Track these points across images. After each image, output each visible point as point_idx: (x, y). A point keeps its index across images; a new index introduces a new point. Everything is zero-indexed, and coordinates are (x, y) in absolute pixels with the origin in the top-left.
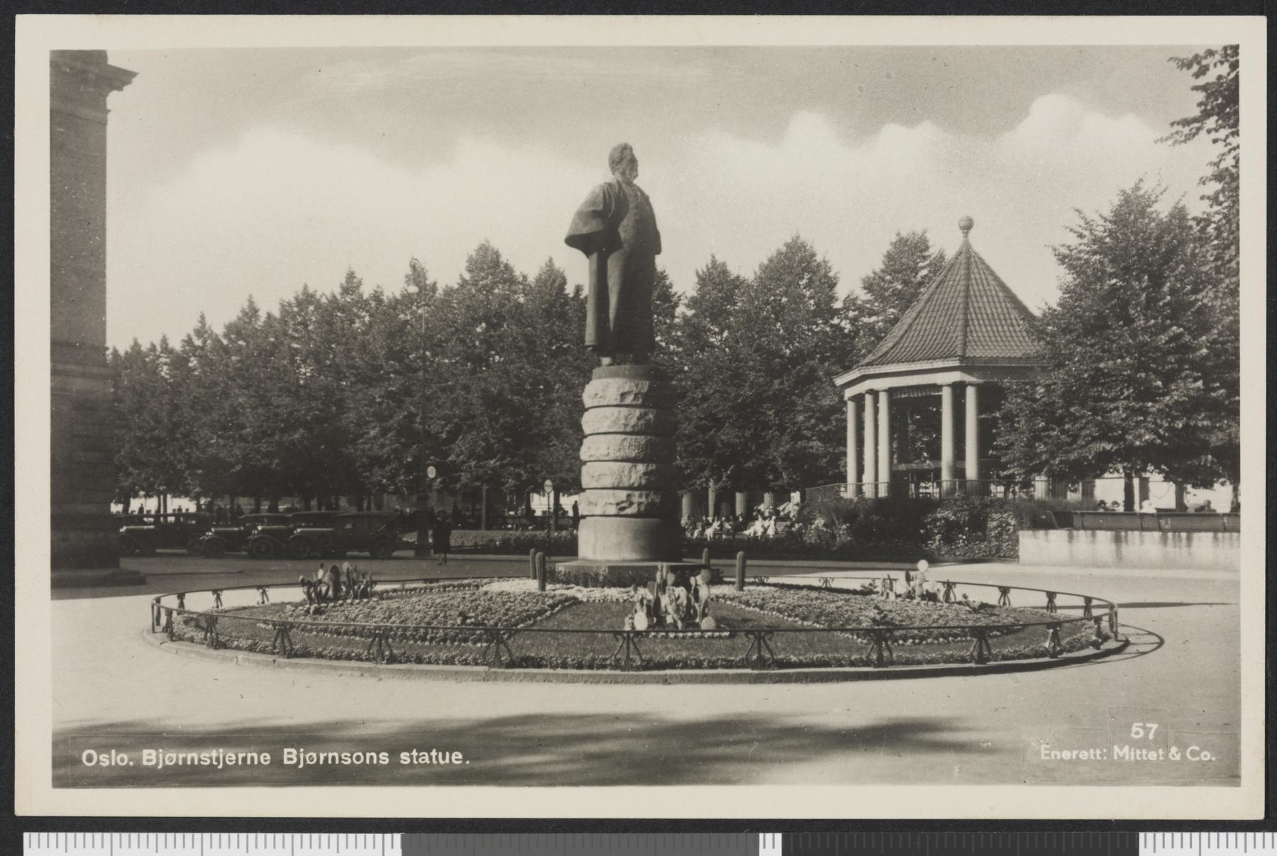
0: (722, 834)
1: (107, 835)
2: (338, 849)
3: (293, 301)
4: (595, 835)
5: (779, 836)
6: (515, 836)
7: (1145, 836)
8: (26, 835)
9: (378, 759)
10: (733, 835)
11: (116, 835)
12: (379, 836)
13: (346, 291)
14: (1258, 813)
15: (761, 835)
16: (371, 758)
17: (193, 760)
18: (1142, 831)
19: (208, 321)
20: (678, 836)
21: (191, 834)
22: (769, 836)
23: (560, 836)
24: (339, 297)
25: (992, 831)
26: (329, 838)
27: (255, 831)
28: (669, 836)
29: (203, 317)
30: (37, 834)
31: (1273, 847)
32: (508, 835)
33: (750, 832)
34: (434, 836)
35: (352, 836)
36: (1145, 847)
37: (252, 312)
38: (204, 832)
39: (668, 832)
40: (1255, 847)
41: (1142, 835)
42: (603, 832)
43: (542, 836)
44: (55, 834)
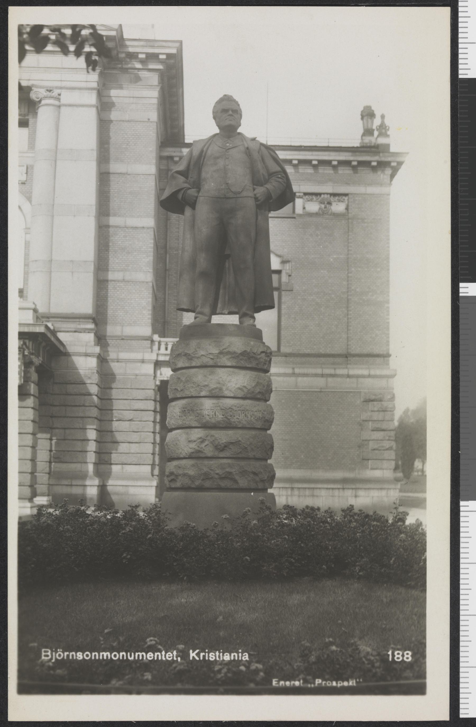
0: (460, 318)
1: (461, 670)
2: (469, 537)
5: (461, 285)
8: (461, 716)
9: (76, 656)
10: (461, 311)
11: (461, 664)
12: (462, 514)
14: (447, 10)
15: (461, 295)
16: (95, 655)
17: (107, 657)
18: (458, 76)
20: (461, 342)
22: (461, 290)
23: (461, 410)
25: (458, 162)
26: (463, 558)
27: (459, 584)
28: (461, 347)
30: (461, 617)
32: (461, 440)
33: (459, 301)
34: (461, 483)
35: (462, 530)
36: (467, 74)
38: (459, 645)
39: (459, 348)
41: (460, 77)
42: (459, 385)
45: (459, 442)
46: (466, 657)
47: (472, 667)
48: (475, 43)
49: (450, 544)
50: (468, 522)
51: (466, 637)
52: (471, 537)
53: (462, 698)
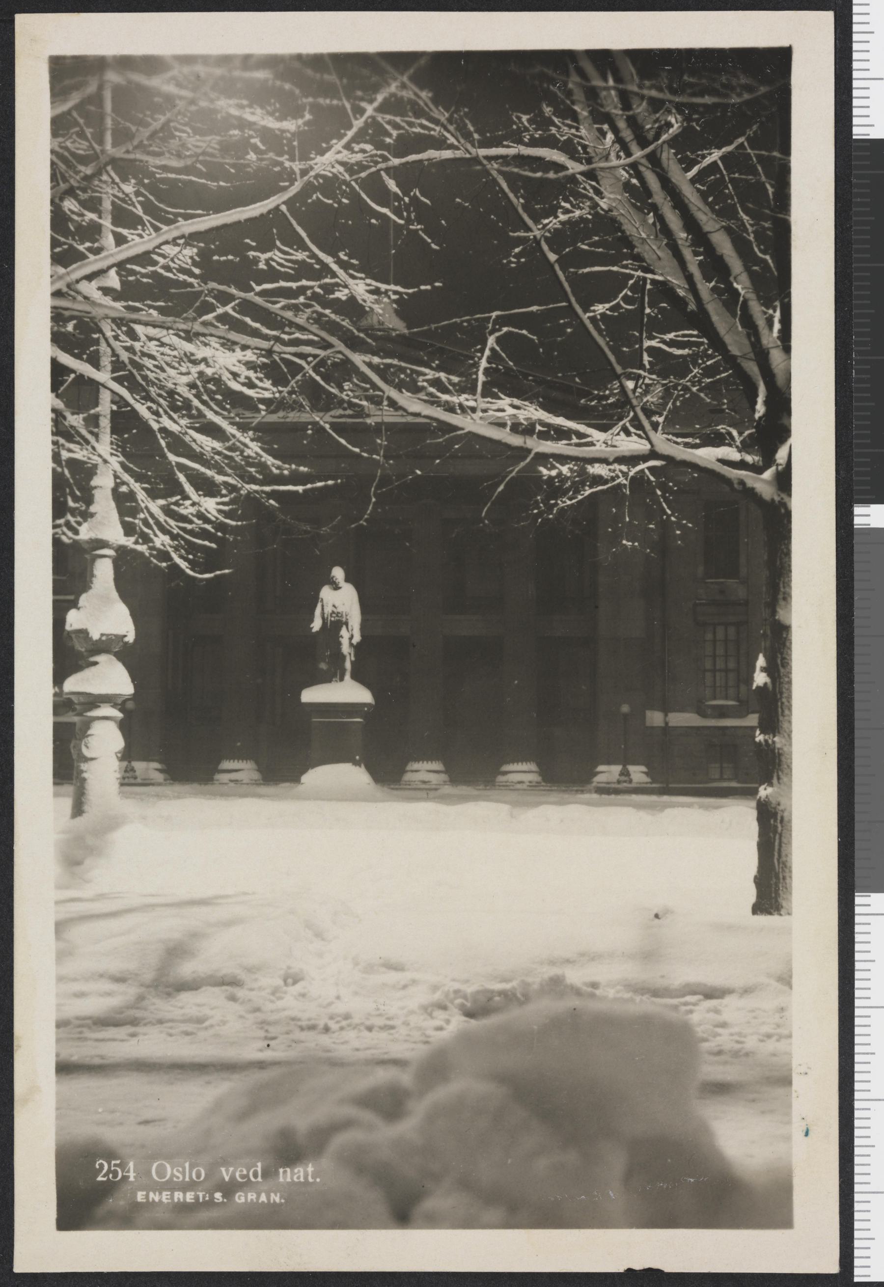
0: (856, 773)
3: (125, 764)
5: (858, 510)
7: (857, 1276)
14: (826, 19)
21: (856, 982)
22: (857, 521)
27: (853, 1072)
31: (869, 979)
40: (868, 51)
44: (856, 1000)
45: (853, 761)
47: (880, 1100)
48: (882, 79)
49: (834, 488)
50: (868, 70)
51: (864, 1185)
52: (874, 961)
53: (858, 970)
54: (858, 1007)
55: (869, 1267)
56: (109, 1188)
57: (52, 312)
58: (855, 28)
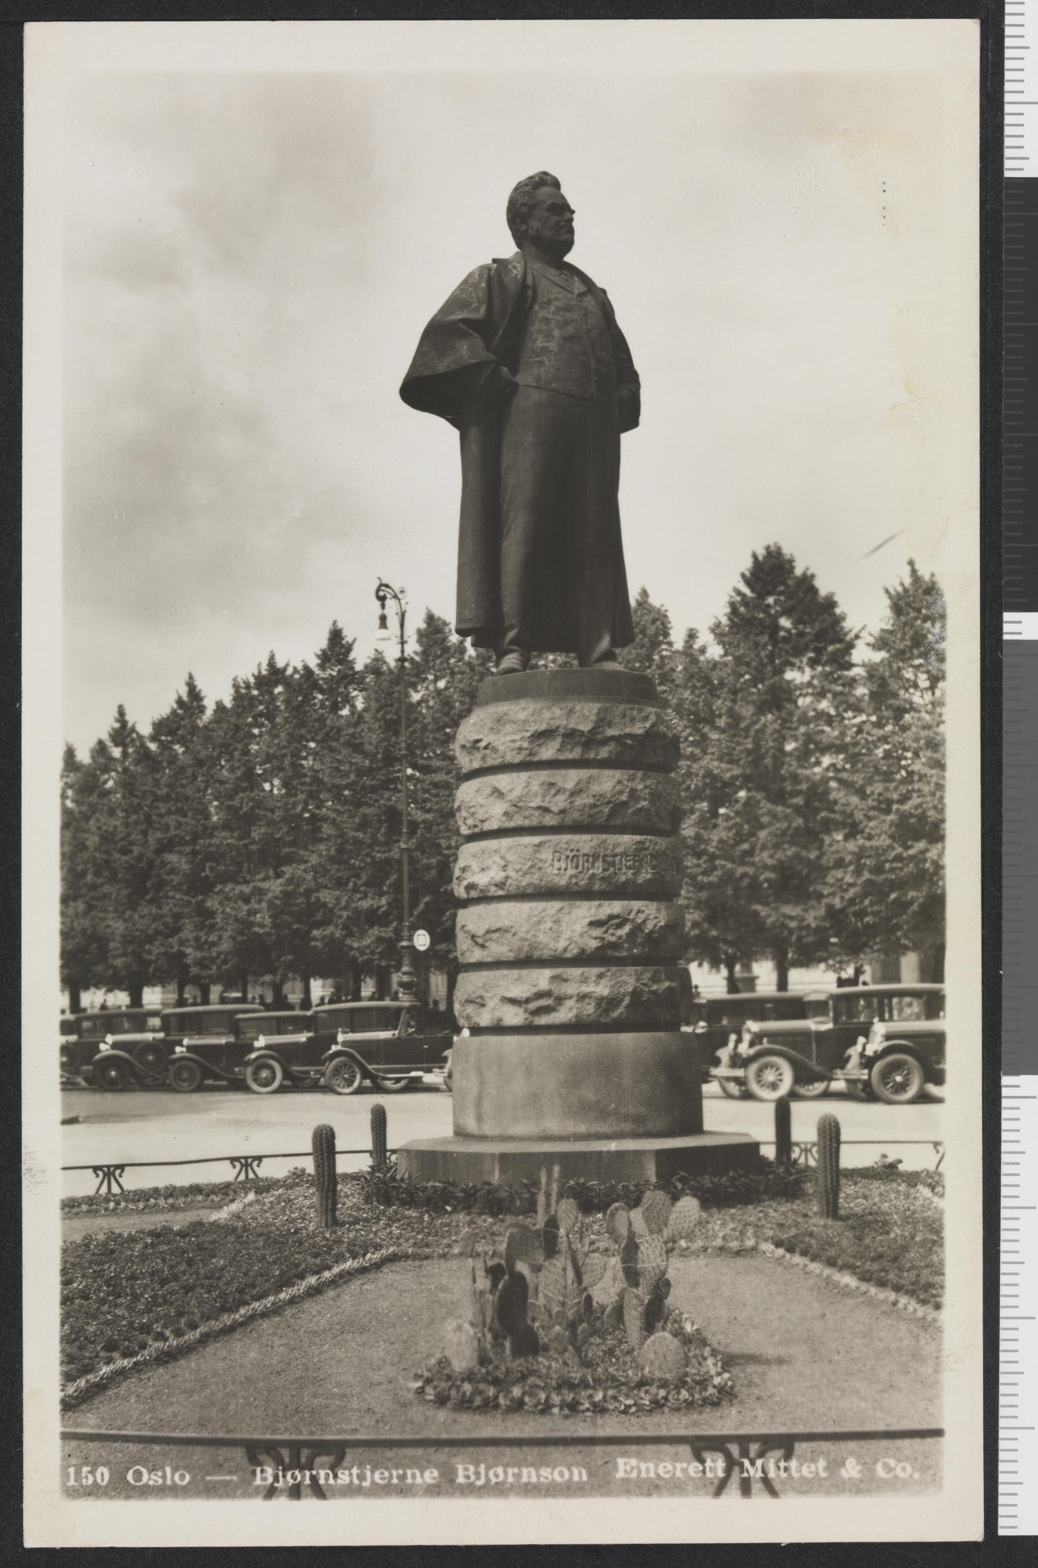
2: (1020, 1153)
3: (252, 680)
4: (1005, 839)
5: (1007, 616)
6: (1005, 937)
7: (1003, 1527)
12: (1005, 1103)
13: (325, 658)
15: (1005, 637)
19: (130, 718)
22: (1006, 628)
24: (317, 671)
27: (998, 1252)
29: (121, 712)
30: (1000, 1420)
32: (1004, 946)
33: (1001, 651)
36: (1021, 169)
37: (194, 697)
41: (1007, 174)
42: (1001, 830)
43: (1006, 904)
46: (1013, 1406)
52: (1034, 1318)
54: (1006, 1141)
55: (1022, 70)
56: (256, 678)
57: (62, 1076)
58: (1007, 98)
